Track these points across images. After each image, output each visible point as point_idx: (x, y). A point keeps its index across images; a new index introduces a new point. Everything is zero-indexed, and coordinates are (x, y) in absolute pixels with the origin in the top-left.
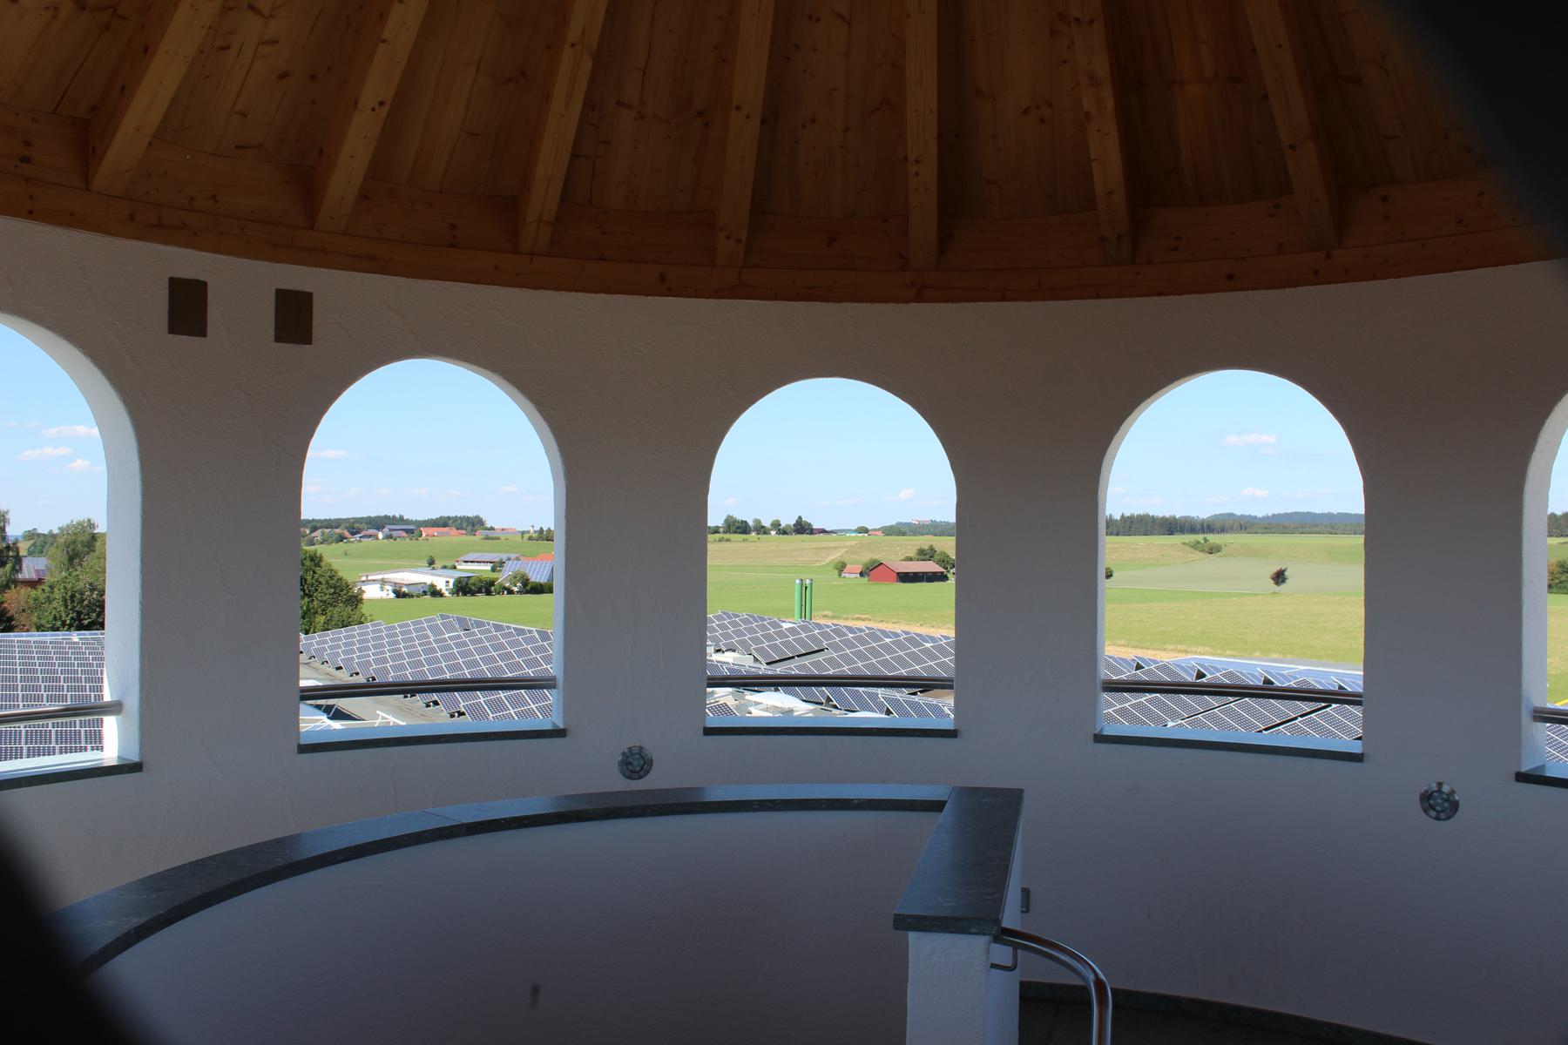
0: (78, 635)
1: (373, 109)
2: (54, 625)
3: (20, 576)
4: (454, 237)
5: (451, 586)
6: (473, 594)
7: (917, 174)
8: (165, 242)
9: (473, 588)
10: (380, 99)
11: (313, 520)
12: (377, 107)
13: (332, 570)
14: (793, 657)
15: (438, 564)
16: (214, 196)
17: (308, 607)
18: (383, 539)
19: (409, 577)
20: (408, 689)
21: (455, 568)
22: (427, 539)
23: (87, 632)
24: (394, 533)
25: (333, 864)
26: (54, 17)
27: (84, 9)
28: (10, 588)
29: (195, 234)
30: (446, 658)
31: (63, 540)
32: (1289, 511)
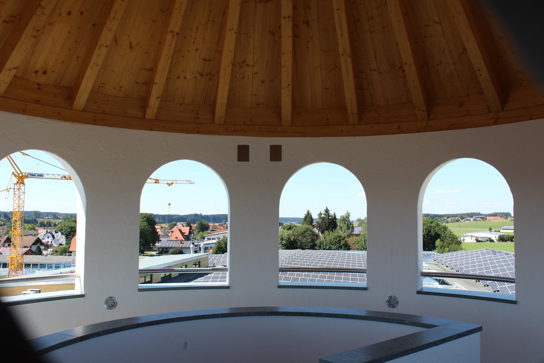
1: (287, 87)
2: (362, 249)
3: (354, 233)
4: (328, 122)
5: (497, 238)
6: (506, 241)
7: (481, 75)
8: (236, 135)
9: (506, 239)
10: (288, 84)
11: (448, 214)
12: (288, 86)
13: (451, 232)
15: (493, 230)
16: (251, 120)
17: (442, 244)
18: (473, 221)
19: (482, 235)
20: (478, 278)
21: (499, 231)
22: (489, 221)
24: (477, 219)
25: (217, 318)
26: (196, 80)
27: (203, 76)
28: (350, 237)
29: (245, 132)
30: (493, 267)
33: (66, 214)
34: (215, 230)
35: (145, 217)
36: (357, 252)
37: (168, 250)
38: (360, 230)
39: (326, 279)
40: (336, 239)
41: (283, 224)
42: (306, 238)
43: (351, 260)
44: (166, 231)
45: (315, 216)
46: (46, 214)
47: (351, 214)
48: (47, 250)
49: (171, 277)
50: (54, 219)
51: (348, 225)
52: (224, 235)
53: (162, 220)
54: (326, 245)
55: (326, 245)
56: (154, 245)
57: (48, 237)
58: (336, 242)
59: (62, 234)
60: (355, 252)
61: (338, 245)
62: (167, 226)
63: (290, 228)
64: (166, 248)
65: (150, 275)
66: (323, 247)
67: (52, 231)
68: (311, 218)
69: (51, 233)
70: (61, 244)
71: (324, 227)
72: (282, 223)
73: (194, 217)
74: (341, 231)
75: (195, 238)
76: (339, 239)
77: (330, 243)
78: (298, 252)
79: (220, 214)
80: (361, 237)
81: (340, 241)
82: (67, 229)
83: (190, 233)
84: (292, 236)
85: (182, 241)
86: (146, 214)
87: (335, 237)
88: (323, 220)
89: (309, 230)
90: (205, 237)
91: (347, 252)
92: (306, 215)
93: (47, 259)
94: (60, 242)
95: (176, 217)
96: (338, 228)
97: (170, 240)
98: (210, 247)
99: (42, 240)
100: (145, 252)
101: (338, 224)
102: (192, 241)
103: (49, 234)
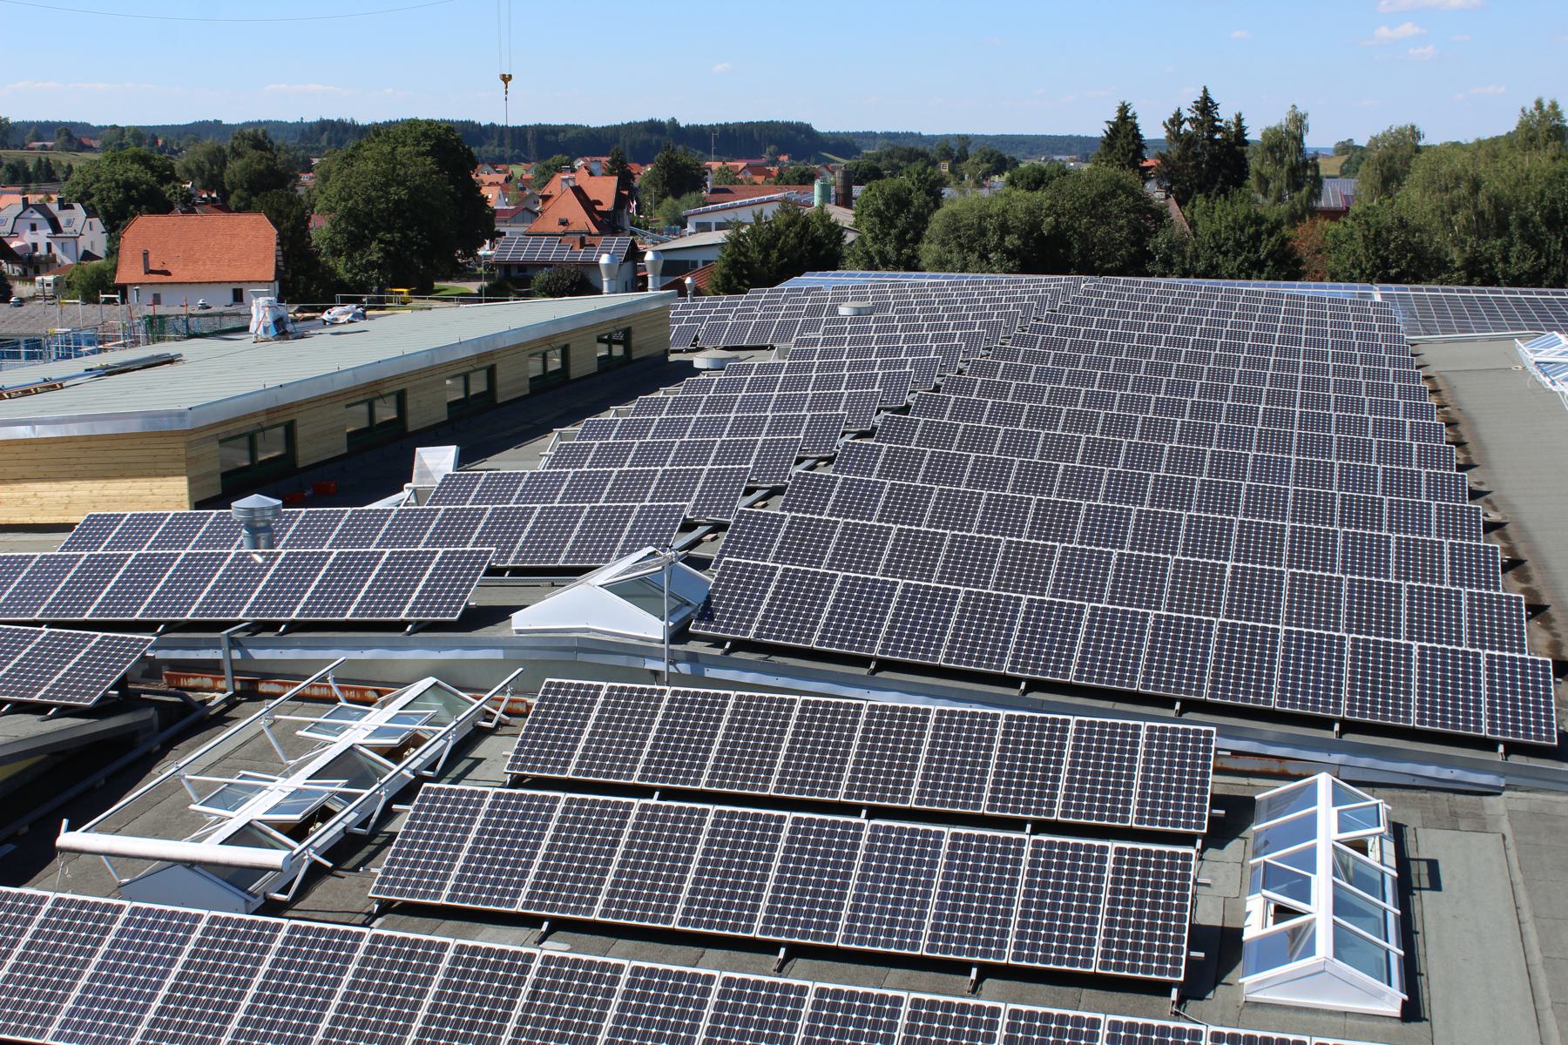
0: (1381, 289)
2: (1352, 274)
3: (1323, 204)
14: (1489, 745)
23: (1393, 286)
31: (1376, 155)
32: (765, 120)
33: (115, 127)
34: (730, 187)
35: (425, 135)
36: (1331, 288)
37: (529, 273)
38: (1350, 193)
39: (1196, 399)
40: (1242, 229)
41: (1016, 164)
42: (1109, 224)
43: (1304, 327)
44: (528, 192)
45: (1152, 129)
46: (32, 131)
47: (1309, 121)
48: (32, 281)
49: (568, 376)
50: (68, 150)
51: (1293, 171)
52: (757, 209)
53: (513, 148)
54: (1196, 257)
55: (1196, 257)
56: (471, 251)
57: (33, 228)
58: (1238, 244)
59: (91, 212)
60: (1325, 288)
61: (1246, 259)
62: (529, 176)
63: (1038, 181)
64: (523, 267)
65: (484, 372)
66: (1183, 263)
67: (50, 199)
68: (1138, 136)
69: (41, 209)
70: (88, 256)
71: (1191, 179)
72: (1013, 159)
73: (643, 137)
74: (1265, 195)
75: (647, 221)
76: (1252, 230)
77: (1212, 249)
78: (1066, 287)
79: (752, 123)
80: (1349, 222)
81: (1256, 237)
82: (109, 190)
83: (621, 202)
84: (1047, 216)
85: (587, 237)
86: (430, 123)
87: (1235, 220)
88: (1188, 148)
89: (1123, 188)
90: (686, 217)
91: (1285, 286)
92: (1113, 123)
93: (22, 317)
94: (84, 244)
95: (570, 134)
96: (1252, 181)
97: (540, 230)
98: (705, 263)
99: (7, 240)
100: (437, 285)
101: (1254, 165)
102: (633, 233)
103: (37, 215)
